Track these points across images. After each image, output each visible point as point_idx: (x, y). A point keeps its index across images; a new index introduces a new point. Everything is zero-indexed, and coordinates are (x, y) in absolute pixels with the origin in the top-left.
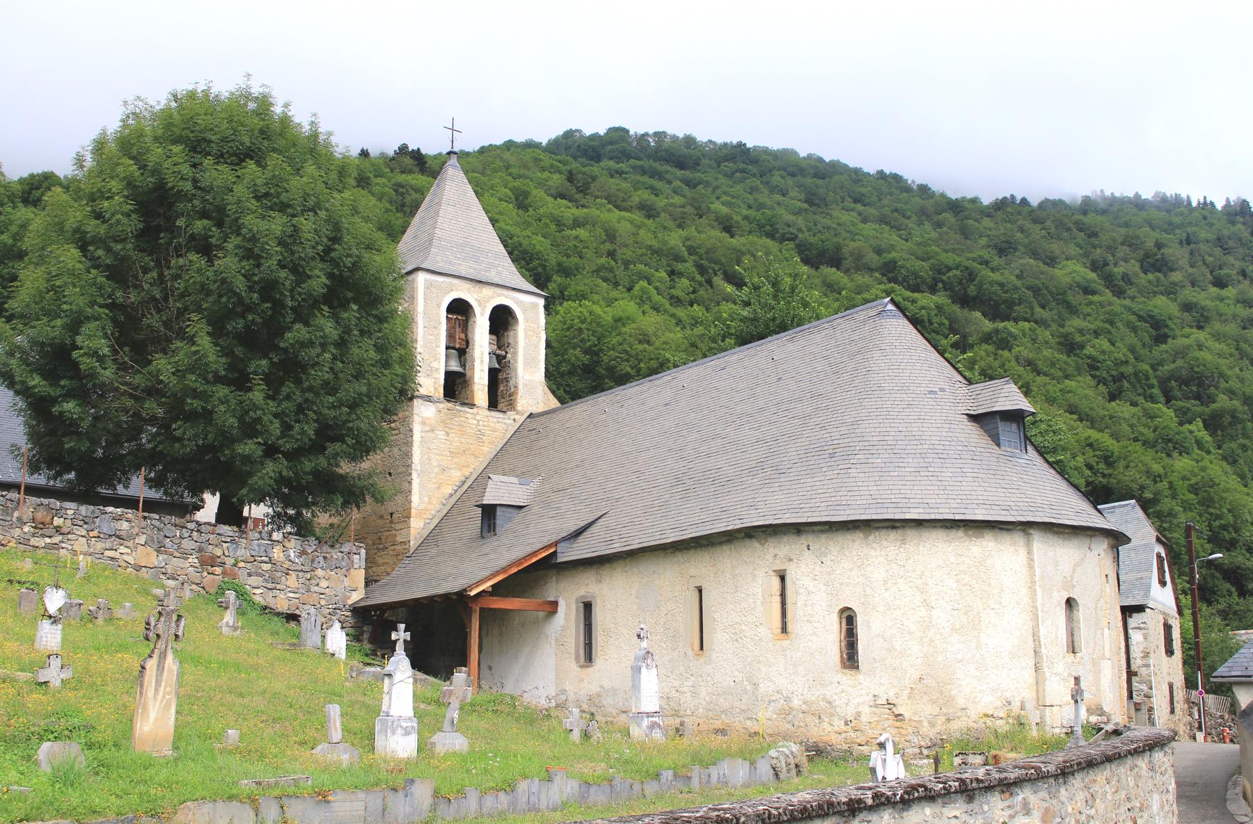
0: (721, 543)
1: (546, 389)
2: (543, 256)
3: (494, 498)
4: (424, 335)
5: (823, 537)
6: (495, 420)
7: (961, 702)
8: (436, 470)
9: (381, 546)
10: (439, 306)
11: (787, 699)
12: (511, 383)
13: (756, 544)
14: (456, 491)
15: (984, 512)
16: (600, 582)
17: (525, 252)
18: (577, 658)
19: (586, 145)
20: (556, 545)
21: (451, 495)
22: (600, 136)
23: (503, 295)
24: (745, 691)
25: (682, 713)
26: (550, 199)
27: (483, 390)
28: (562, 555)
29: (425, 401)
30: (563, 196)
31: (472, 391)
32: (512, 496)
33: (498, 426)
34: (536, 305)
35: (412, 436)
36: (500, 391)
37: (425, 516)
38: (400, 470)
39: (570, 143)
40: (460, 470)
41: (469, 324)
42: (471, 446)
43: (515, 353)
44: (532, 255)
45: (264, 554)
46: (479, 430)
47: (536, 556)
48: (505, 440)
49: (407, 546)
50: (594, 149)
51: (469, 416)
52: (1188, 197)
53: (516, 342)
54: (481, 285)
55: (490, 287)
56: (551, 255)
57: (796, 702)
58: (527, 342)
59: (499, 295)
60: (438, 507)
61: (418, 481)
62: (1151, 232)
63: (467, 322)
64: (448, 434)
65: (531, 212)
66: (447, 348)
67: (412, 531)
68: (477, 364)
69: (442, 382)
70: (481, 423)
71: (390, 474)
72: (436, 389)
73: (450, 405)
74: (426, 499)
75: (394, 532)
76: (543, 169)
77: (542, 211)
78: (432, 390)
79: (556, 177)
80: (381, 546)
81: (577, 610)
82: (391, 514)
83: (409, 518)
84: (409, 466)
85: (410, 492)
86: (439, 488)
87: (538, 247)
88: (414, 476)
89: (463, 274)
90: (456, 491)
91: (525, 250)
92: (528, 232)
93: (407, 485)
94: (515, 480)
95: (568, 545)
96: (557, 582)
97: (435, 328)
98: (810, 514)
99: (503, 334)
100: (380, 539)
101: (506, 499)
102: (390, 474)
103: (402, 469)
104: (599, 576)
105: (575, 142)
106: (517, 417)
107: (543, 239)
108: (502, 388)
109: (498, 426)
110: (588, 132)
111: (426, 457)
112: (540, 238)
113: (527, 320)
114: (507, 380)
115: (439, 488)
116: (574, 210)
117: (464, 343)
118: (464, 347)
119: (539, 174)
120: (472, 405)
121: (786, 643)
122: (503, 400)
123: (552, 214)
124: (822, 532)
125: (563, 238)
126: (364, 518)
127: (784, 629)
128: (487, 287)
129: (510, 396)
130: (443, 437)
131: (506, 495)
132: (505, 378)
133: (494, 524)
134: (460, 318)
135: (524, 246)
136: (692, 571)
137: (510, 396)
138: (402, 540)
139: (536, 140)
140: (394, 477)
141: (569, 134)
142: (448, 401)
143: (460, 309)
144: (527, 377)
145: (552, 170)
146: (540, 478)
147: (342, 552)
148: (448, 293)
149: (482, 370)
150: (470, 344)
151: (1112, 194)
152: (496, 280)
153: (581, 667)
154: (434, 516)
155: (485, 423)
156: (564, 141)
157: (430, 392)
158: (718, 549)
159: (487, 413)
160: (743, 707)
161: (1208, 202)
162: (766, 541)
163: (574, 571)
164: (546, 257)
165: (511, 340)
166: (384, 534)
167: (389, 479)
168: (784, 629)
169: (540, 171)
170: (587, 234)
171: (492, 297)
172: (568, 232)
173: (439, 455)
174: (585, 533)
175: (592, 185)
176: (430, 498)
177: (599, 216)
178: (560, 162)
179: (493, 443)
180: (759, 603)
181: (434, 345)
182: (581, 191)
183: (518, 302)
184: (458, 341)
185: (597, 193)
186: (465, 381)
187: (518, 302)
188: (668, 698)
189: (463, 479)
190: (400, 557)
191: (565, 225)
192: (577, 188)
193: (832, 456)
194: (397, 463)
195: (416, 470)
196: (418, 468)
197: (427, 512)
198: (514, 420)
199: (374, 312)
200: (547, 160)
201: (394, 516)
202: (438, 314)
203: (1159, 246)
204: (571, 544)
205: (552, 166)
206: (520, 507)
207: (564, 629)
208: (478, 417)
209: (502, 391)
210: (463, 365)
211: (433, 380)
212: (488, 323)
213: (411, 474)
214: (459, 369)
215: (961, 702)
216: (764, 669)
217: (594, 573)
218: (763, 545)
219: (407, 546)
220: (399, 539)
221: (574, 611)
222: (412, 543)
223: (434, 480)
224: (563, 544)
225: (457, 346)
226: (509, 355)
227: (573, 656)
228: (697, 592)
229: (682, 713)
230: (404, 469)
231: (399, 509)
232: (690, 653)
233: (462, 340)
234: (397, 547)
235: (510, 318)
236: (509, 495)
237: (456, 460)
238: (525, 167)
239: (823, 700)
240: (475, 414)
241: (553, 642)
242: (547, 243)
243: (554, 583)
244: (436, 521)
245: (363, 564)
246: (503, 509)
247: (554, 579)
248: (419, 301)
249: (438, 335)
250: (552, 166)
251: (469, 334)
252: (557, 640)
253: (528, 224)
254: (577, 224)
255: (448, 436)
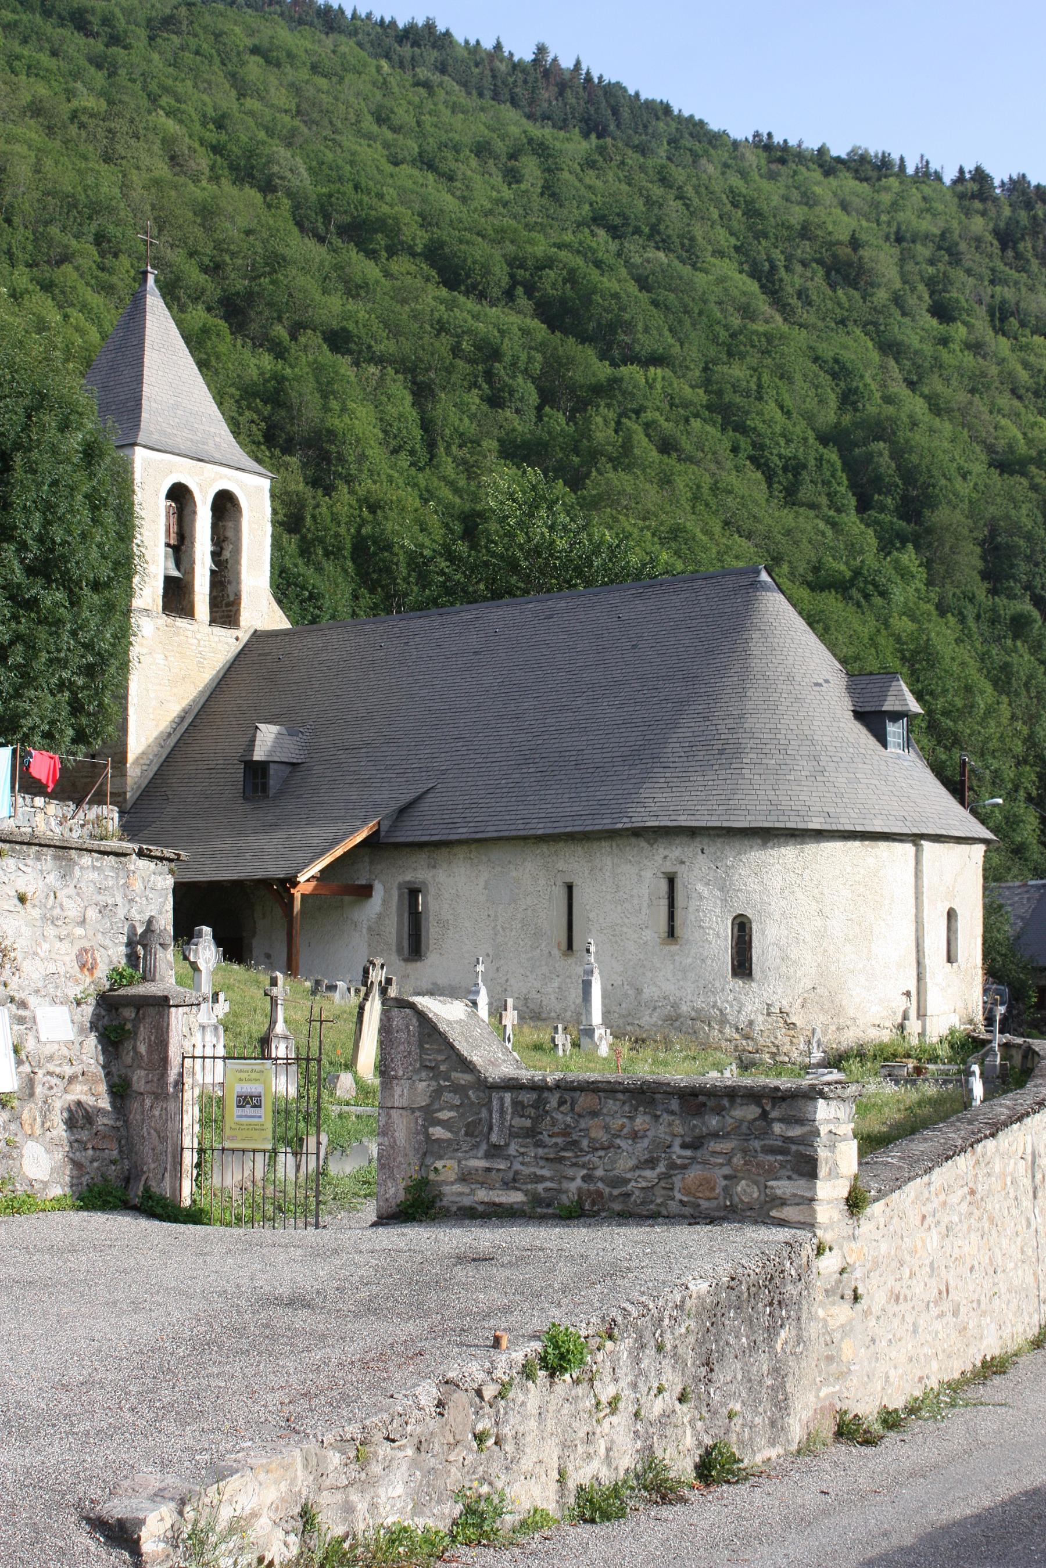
0: (599, 839)
5: (719, 842)
7: (851, 1012)
11: (675, 1006)
13: (643, 844)
15: (881, 822)
16: (434, 867)
18: (400, 951)
24: (626, 996)
25: (544, 1016)
34: (260, 489)
45: (27, 824)
51: (189, 634)
52: (902, 159)
57: (684, 1008)
62: (845, 218)
69: (161, 591)
81: (400, 896)
89: (183, 448)
96: (371, 863)
98: (708, 818)
121: (674, 948)
124: (719, 836)
127: (671, 932)
136: (561, 865)
143: (179, 495)
151: (785, 141)
153: (406, 960)
158: (595, 845)
160: (624, 1012)
161: (932, 170)
162: (656, 841)
168: (671, 932)
180: (645, 905)
188: (526, 999)
193: (721, 752)
203: (855, 243)
207: (380, 917)
212: (210, 514)
215: (851, 1012)
216: (649, 974)
218: (652, 845)
221: (395, 898)
222: (128, 795)
227: (394, 948)
228: (566, 890)
229: (544, 1016)
232: (556, 952)
235: (229, 505)
239: (713, 1007)
241: (364, 931)
247: (367, 859)
252: (370, 929)
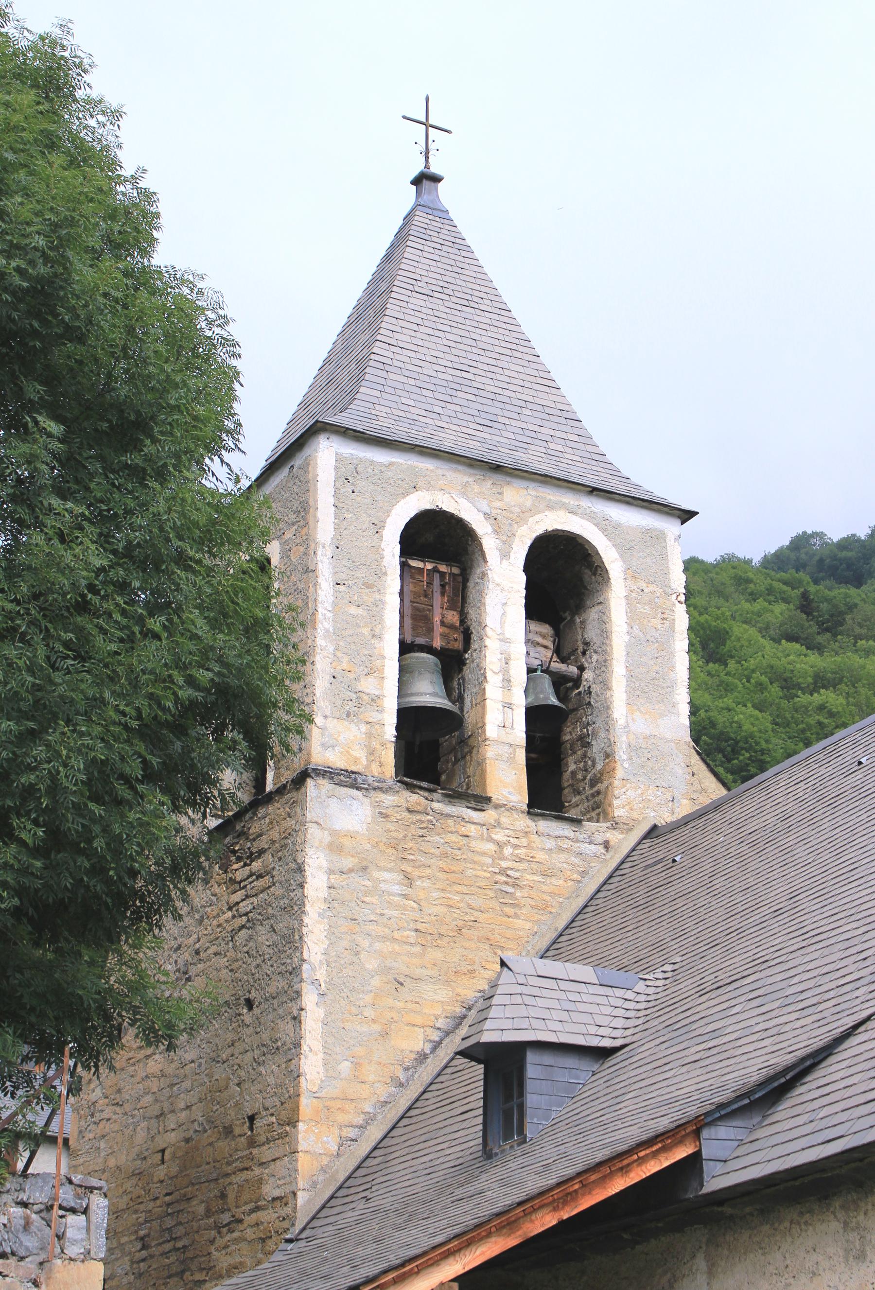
1: (696, 760)
2: (757, 743)
3: (517, 1024)
4: (335, 604)
6: (550, 844)
8: (376, 982)
9: (226, 1218)
10: (378, 529)
12: (597, 746)
14: (437, 1045)
17: (723, 737)
19: (834, 557)
20: (697, 1133)
21: (422, 1057)
22: (859, 540)
23: (564, 506)
26: (766, 643)
27: (511, 760)
28: (719, 1168)
29: (340, 784)
30: (791, 638)
31: (481, 764)
32: (576, 1017)
33: (559, 860)
35: (301, 886)
36: (566, 775)
37: (341, 1118)
38: (272, 990)
39: (803, 556)
40: (448, 982)
41: (471, 584)
42: (481, 917)
43: (604, 665)
44: (737, 742)
46: (503, 872)
47: (625, 1170)
48: (581, 902)
49: (288, 1210)
50: (849, 564)
51: (472, 830)
53: (605, 634)
54: (498, 478)
55: (525, 483)
56: (774, 740)
58: (636, 630)
59: (550, 507)
60: (383, 1091)
61: (320, 1012)
63: (465, 581)
64: (409, 880)
65: (732, 665)
66: (405, 648)
67: (304, 1163)
68: (493, 690)
69: (390, 732)
70: (508, 851)
71: (249, 1004)
72: (371, 752)
73: (415, 799)
74: (345, 1067)
75: (257, 1171)
76: (753, 597)
77: (752, 663)
78: (361, 755)
79: (779, 608)
80: (226, 1218)
82: (252, 1119)
83: (293, 1122)
84: (295, 971)
85: (298, 1045)
86: (385, 1034)
87: (747, 726)
88: (309, 999)
89: (447, 441)
90: (437, 1045)
91: (722, 733)
92: (728, 701)
93: (289, 1026)
94: (585, 972)
95: (741, 1134)
97: (369, 586)
99: (572, 621)
100: (223, 1196)
101: (557, 1026)
102: (249, 1004)
103: (279, 984)
104: (853, 1236)
105: (814, 555)
106: (614, 837)
107: (757, 712)
108: (572, 767)
109: (559, 860)
110: (835, 535)
111: (345, 943)
112: (750, 710)
113: (632, 574)
114: (584, 742)
115: (385, 1034)
116: (813, 658)
117: (460, 637)
118: (459, 645)
119: (747, 606)
120: (481, 801)
122: (575, 799)
123: (772, 667)
125: (796, 711)
126: (187, 1140)
128: (518, 483)
129: (594, 782)
130: (396, 889)
131: (555, 1015)
132: (581, 738)
133: (521, 1108)
134: (443, 568)
135: (720, 726)
137: (592, 785)
138: (277, 1193)
139: (741, 555)
140: (257, 1011)
141: (800, 542)
142: (410, 787)
144: (641, 726)
145: (772, 598)
146: (668, 968)
147: (25, 1205)
148: (405, 494)
149: (508, 706)
150: (474, 637)
152: (545, 467)
154: (370, 1119)
155: (521, 852)
156: (793, 556)
157: (356, 761)
159: (524, 822)
163: (766, 1228)
164: (764, 745)
165: (591, 634)
166: (235, 1179)
167: (248, 1018)
169: (747, 601)
170: (842, 700)
171: (532, 511)
172: (803, 699)
173: (384, 938)
174: (801, 1089)
175: (848, 617)
176: (357, 1065)
177: (863, 667)
178: (785, 583)
179: (544, 907)
181: (366, 631)
182: (827, 630)
183: (605, 526)
184: (438, 630)
185: (858, 630)
186: (463, 741)
187: (605, 526)
189: (459, 1010)
190: (271, 1245)
191: (798, 686)
192: (820, 624)
194: (266, 969)
195: (315, 982)
196: (321, 975)
197: (349, 1106)
198: (606, 845)
199: (128, 459)
200: (761, 584)
201: (258, 1123)
202: (376, 549)
204: (752, 1130)
205: (770, 591)
206: (602, 1054)
208: (499, 836)
209: (574, 773)
210: (456, 695)
211: (364, 728)
212: (522, 579)
213: (298, 994)
214: (440, 701)
217: (835, 1225)
219: (288, 1210)
220: (270, 1190)
222: (302, 1198)
223: (369, 1013)
224: (722, 1131)
225: (437, 643)
226: (588, 675)
230: (282, 984)
231: (268, 1103)
233: (452, 627)
234: (264, 1216)
236: (564, 1016)
237: (434, 955)
238: (720, 593)
240: (490, 827)
242: (765, 719)
243: (701, 1279)
244: (375, 1133)
245: (99, 1244)
246: (548, 1058)
247: (701, 1263)
248: (320, 514)
249: (379, 604)
250: (770, 591)
251: (472, 613)
253: (728, 688)
254: (820, 682)
255: (411, 886)
